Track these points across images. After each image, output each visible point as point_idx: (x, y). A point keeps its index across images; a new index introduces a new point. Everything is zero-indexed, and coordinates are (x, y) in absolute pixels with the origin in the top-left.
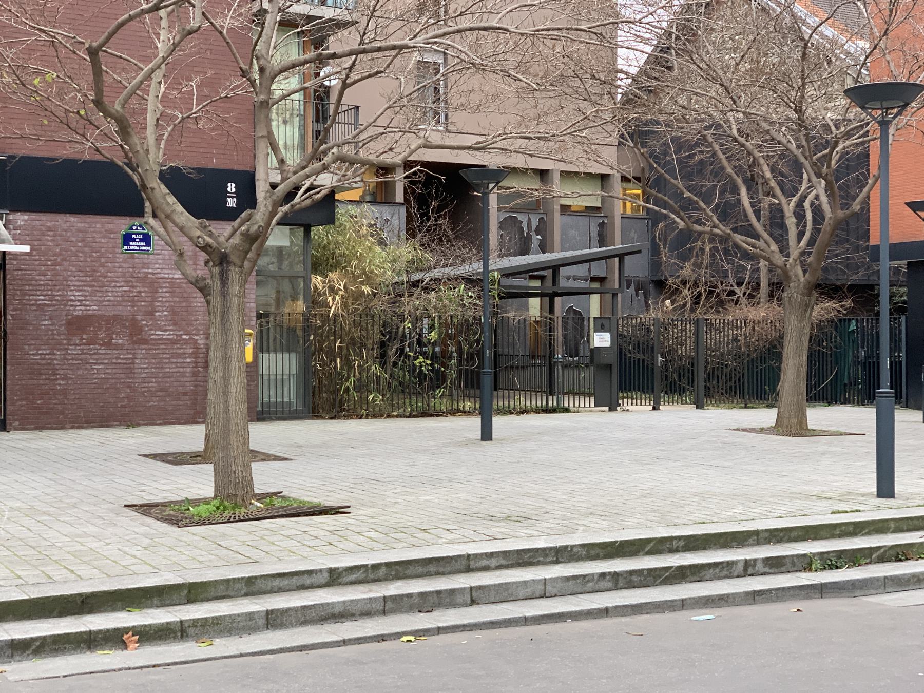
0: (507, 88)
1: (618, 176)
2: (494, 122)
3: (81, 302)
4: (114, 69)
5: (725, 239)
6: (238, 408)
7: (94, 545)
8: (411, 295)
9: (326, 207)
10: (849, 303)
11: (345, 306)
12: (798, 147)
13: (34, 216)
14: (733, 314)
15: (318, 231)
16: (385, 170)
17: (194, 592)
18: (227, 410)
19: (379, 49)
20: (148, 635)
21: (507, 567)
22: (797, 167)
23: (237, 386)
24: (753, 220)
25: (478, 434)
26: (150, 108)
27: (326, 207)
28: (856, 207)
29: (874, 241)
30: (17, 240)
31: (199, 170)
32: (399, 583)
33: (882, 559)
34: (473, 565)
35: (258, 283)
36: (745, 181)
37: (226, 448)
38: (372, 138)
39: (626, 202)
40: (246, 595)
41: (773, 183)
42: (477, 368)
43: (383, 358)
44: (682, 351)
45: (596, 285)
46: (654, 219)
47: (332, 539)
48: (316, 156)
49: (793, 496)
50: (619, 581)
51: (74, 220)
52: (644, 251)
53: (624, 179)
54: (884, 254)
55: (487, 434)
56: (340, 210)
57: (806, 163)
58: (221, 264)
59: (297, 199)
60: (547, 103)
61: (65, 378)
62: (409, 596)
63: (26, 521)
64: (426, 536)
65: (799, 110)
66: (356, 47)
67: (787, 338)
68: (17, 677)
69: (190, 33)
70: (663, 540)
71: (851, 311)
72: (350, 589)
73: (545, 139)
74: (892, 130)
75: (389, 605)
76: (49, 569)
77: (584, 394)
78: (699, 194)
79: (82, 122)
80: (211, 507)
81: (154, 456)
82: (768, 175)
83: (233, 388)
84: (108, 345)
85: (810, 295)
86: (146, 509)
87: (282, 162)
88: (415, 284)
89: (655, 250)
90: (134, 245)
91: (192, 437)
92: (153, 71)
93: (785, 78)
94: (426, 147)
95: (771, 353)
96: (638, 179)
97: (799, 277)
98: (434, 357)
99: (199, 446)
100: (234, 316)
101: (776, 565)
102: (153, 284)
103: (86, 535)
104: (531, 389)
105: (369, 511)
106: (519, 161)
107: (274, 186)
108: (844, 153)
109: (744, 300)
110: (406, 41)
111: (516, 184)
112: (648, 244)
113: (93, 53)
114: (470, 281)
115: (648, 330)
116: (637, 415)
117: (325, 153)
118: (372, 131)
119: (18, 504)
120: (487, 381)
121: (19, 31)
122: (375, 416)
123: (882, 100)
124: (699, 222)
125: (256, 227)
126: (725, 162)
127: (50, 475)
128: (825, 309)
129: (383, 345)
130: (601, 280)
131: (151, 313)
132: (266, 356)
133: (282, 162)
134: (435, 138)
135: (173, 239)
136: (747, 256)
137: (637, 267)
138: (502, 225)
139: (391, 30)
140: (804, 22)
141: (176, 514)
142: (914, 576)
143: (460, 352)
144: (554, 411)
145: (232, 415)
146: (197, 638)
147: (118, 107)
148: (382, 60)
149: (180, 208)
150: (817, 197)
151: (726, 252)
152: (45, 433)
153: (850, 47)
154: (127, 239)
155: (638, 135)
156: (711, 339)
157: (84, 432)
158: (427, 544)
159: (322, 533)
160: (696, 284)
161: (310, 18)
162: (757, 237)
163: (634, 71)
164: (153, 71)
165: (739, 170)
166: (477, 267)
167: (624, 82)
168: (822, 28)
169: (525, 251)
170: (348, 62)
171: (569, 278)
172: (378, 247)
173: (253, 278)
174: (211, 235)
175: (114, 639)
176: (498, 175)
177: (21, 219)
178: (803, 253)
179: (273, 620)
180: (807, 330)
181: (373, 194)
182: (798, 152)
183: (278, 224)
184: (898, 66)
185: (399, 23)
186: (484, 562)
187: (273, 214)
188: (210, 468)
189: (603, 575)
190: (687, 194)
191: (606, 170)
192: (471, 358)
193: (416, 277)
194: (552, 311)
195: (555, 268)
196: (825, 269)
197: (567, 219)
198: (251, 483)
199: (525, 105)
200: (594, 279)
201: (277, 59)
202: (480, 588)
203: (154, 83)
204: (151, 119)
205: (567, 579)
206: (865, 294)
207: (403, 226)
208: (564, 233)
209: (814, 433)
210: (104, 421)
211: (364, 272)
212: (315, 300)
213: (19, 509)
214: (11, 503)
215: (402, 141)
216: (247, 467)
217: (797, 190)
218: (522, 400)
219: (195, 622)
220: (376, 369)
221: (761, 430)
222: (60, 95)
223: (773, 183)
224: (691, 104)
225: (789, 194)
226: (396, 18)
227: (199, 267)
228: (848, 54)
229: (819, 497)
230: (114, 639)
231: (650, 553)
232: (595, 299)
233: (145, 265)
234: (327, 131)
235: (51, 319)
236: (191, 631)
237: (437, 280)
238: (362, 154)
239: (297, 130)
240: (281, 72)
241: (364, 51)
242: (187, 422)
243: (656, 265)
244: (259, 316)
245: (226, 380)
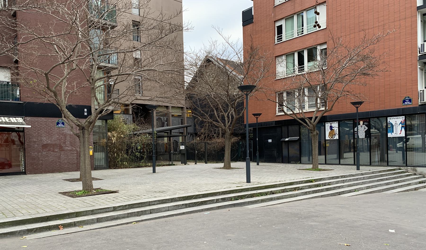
0: (157, 85)
1: (185, 107)
2: (154, 94)
3: (46, 140)
4: (53, 79)
5: (211, 123)
6: (88, 167)
7: (50, 203)
8: (134, 137)
9: (111, 115)
10: (240, 138)
11: (117, 140)
12: (228, 101)
13: (32, 118)
14: (214, 141)
15: (109, 121)
16: (127, 105)
17: (78, 214)
18: (85, 167)
19: (123, 75)
20: (65, 226)
21: (159, 204)
22: (227, 106)
23: (88, 161)
24: (218, 118)
25: (152, 172)
26: (63, 89)
27: (111, 115)
28: (241, 115)
29: (245, 123)
30: (27, 124)
31: (77, 106)
32: (132, 209)
33: (248, 197)
34: (151, 204)
35: (93, 135)
36: (216, 109)
37: (85, 177)
38: (122, 97)
39: (188, 113)
40: (91, 214)
41: (222, 109)
42: (152, 155)
43: (127, 153)
44: (202, 150)
45: (181, 134)
46: (194, 118)
47: (114, 199)
48: (108, 102)
49: (228, 183)
50: (187, 206)
51: (43, 119)
52: (192, 126)
53: (187, 108)
54: (247, 126)
55: (154, 171)
56: (116, 116)
57: (229, 105)
58: (82, 129)
59: (103, 113)
60: (167, 89)
61: (42, 160)
62: (134, 212)
63: (32, 198)
64: (138, 197)
65: (227, 92)
66: (117, 74)
67: (226, 146)
68: (29, 239)
69: (73, 70)
70: (197, 195)
71: (240, 140)
72: (119, 211)
73: (167, 98)
74: (249, 97)
75: (129, 215)
76: (38, 210)
77: (178, 161)
78: (205, 112)
79: (44, 93)
80: (82, 193)
81: (67, 180)
82: (221, 107)
83: (87, 162)
84: (53, 151)
85: (231, 136)
86: (64, 194)
87: (99, 103)
88: (135, 134)
89: (195, 126)
90: (60, 125)
91: (77, 175)
92: (63, 80)
93: (224, 84)
94: (136, 99)
95: (223, 150)
96: (190, 108)
97: (228, 132)
98: (140, 152)
99: (79, 177)
100: (86, 143)
101: (224, 200)
102: (65, 135)
103: (48, 201)
104: (165, 160)
105: (124, 192)
106: (160, 104)
107: (96, 109)
108: (238, 102)
109: (216, 137)
110: (130, 73)
111: (160, 110)
112: (193, 124)
113: (46, 74)
114: (149, 134)
115: (194, 145)
116: (191, 166)
117: (110, 101)
118: (122, 96)
119: (29, 194)
120: (154, 158)
121: (26, 69)
122: (125, 168)
123: (246, 89)
124: (205, 119)
125: (91, 120)
126: (211, 104)
127: (38, 186)
128: (234, 139)
129: (127, 150)
130: (182, 133)
131: (65, 143)
132: (96, 153)
133: (99, 103)
134: (139, 98)
135: (69, 125)
136: (217, 127)
137: (191, 130)
138: (157, 120)
139: (127, 70)
140: (229, 71)
141: (73, 195)
142: (255, 201)
143: (147, 151)
144: (171, 165)
145: (87, 168)
146: (79, 226)
147: (54, 89)
148: (124, 77)
149: (71, 115)
150: (232, 113)
151: (212, 126)
152: (37, 175)
153: (239, 77)
154: (58, 124)
155: (190, 97)
156: (208, 147)
157: (47, 174)
158: (139, 199)
159: (111, 198)
160: (205, 134)
161: (105, 67)
162: (219, 122)
163: (189, 82)
164: (63, 80)
165: (214, 106)
166: (151, 130)
167: (186, 84)
168: (232, 72)
169: (163, 126)
170: (115, 78)
171: (174, 132)
172: (125, 125)
173: (92, 133)
174: (80, 122)
175: (57, 227)
176: (155, 107)
177: (28, 119)
178: (229, 126)
179: (99, 220)
180: (230, 144)
181: (124, 112)
182: (228, 102)
183: (98, 119)
184: (250, 81)
185: (129, 68)
186: (153, 203)
187: (97, 117)
188: (81, 182)
189: (183, 205)
190: (202, 112)
191: (182, 106)
192: (150, 153)
193: (135, 133)
194: (170, 141)
195: (171, 130)
196: (234, 130)
197: (173, 118)
198: (92, 186)
199: (162, 90)
200: (180, 133)
201: (97, 77)
202: (153, 209)
203: (63, 83)
204: (63, 92)
205: (174, 206)
206: (243, 136)
207: (132, 120)
208: (172, 121)
209: (233, 168)
210: (53, 171)
211: (121, 131)
212: (109, 139)
213: (29, 195)
214: (27, 193)
215: (130, 98)
216: (91, 182)
217: (227, 111)
218: (163, 163)
219: (78, 222)
220: (125, 156)
221: (220, 168)
222: (38, 86)
223: (222, 109)
224: (203, 90)
225: (226, 112)
226: (128, 67)
227: (77, 131)
228: (239, 78)
229: (233, 183)
230: (57, 227)
231: (194, 199)
232: (181, 138)
233: (63, 130)
234: (111, 95)
235: (37, 145)
236: (77, 224)
237: (141, 133)
238: (120, 101)
239: (103, 95)
240: (97, 80)
241: (119, 75)
242: (75, 171)
243: (195, 129)
244: (94, 143)
245: (85, 160)
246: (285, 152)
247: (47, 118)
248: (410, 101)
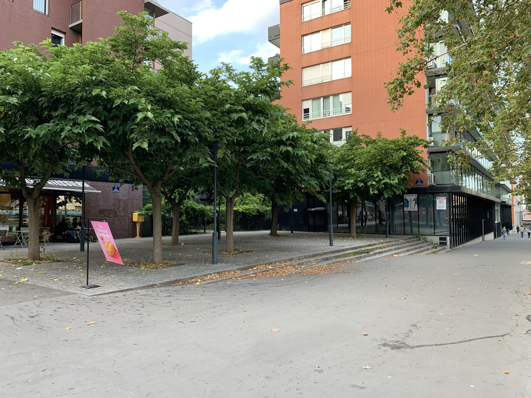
84: (109, 217)
131: (119, 208)
154: (114, 188)
233: (118, 196)
246: (311, 221)
247: (105, 183)
248: (421, 182)
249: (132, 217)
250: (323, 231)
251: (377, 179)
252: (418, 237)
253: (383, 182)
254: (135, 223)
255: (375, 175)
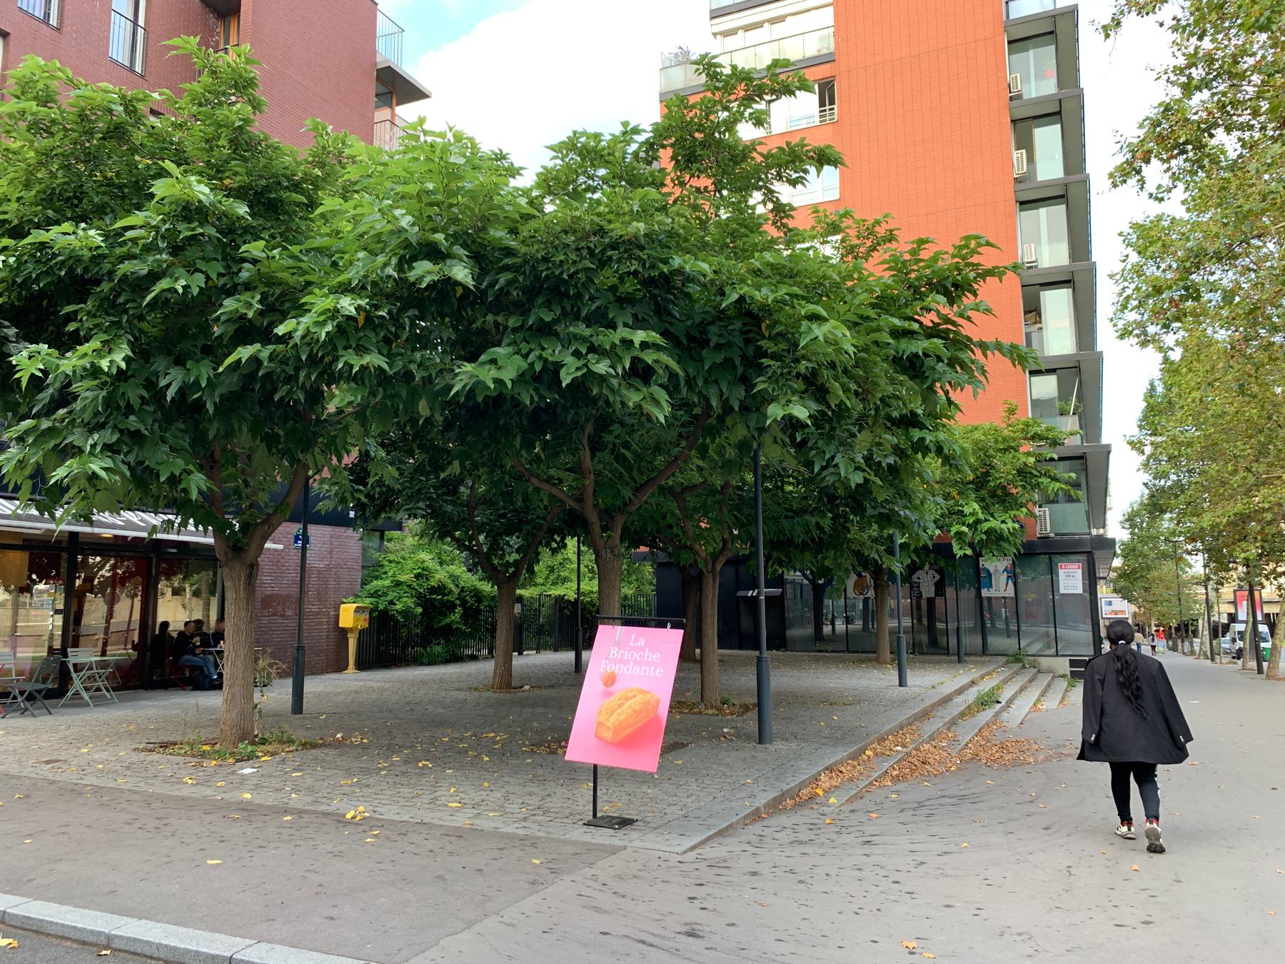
84: (283, 616)
249: (337, 617)
250: (778, 649)
251: (971, 520)
252: (1019, 661)
253: (985, 526)
254: (344, 632)
255: (967, 510)
